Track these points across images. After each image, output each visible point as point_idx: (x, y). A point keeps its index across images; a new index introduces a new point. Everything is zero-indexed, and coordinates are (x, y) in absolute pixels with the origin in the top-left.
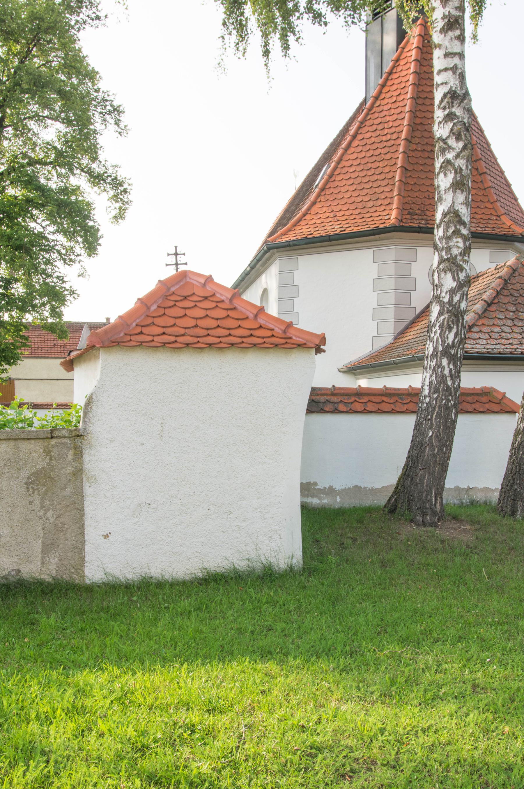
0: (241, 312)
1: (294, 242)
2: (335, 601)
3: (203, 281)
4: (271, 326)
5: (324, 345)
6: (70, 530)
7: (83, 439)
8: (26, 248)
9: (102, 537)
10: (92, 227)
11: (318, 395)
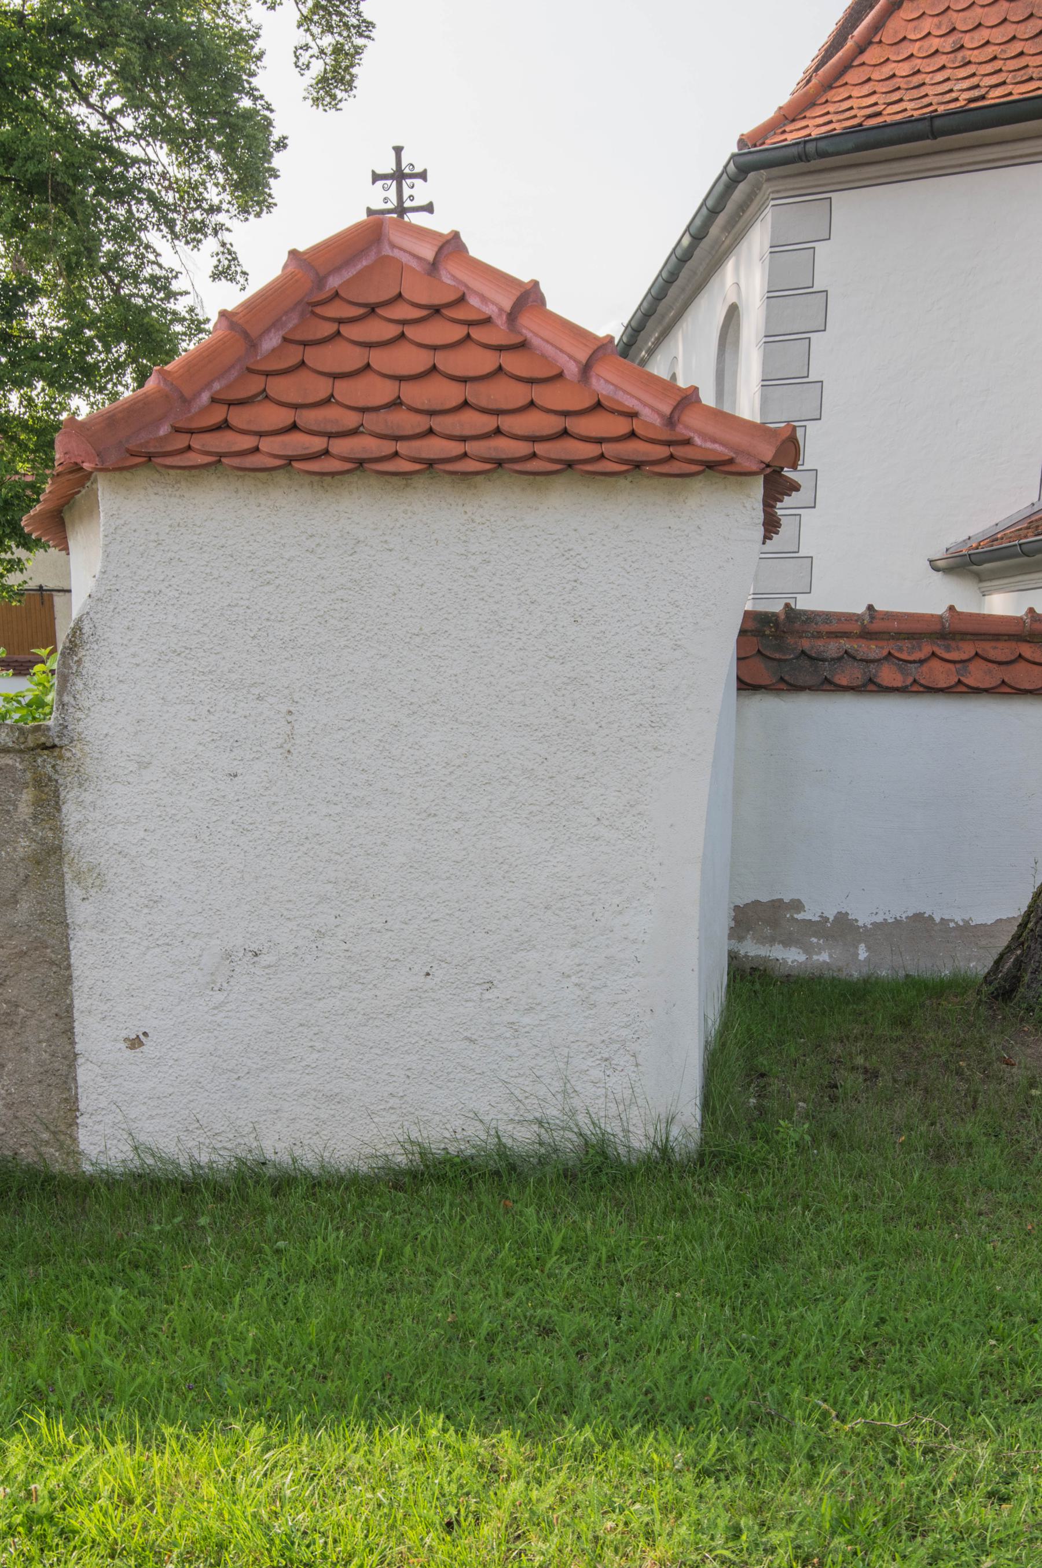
0: (544, 357)
1: (822, 145)
2: (764, 1252)
3: (428, 253)
4: (631, 403)
5: (794, 467)
6: (33, 1022)
7: (61, 757)
8: (56, 185)
9: (123, 1046)
10: (249, 115)
11: (819, 635)
